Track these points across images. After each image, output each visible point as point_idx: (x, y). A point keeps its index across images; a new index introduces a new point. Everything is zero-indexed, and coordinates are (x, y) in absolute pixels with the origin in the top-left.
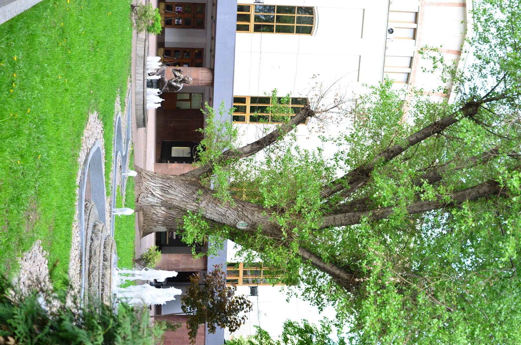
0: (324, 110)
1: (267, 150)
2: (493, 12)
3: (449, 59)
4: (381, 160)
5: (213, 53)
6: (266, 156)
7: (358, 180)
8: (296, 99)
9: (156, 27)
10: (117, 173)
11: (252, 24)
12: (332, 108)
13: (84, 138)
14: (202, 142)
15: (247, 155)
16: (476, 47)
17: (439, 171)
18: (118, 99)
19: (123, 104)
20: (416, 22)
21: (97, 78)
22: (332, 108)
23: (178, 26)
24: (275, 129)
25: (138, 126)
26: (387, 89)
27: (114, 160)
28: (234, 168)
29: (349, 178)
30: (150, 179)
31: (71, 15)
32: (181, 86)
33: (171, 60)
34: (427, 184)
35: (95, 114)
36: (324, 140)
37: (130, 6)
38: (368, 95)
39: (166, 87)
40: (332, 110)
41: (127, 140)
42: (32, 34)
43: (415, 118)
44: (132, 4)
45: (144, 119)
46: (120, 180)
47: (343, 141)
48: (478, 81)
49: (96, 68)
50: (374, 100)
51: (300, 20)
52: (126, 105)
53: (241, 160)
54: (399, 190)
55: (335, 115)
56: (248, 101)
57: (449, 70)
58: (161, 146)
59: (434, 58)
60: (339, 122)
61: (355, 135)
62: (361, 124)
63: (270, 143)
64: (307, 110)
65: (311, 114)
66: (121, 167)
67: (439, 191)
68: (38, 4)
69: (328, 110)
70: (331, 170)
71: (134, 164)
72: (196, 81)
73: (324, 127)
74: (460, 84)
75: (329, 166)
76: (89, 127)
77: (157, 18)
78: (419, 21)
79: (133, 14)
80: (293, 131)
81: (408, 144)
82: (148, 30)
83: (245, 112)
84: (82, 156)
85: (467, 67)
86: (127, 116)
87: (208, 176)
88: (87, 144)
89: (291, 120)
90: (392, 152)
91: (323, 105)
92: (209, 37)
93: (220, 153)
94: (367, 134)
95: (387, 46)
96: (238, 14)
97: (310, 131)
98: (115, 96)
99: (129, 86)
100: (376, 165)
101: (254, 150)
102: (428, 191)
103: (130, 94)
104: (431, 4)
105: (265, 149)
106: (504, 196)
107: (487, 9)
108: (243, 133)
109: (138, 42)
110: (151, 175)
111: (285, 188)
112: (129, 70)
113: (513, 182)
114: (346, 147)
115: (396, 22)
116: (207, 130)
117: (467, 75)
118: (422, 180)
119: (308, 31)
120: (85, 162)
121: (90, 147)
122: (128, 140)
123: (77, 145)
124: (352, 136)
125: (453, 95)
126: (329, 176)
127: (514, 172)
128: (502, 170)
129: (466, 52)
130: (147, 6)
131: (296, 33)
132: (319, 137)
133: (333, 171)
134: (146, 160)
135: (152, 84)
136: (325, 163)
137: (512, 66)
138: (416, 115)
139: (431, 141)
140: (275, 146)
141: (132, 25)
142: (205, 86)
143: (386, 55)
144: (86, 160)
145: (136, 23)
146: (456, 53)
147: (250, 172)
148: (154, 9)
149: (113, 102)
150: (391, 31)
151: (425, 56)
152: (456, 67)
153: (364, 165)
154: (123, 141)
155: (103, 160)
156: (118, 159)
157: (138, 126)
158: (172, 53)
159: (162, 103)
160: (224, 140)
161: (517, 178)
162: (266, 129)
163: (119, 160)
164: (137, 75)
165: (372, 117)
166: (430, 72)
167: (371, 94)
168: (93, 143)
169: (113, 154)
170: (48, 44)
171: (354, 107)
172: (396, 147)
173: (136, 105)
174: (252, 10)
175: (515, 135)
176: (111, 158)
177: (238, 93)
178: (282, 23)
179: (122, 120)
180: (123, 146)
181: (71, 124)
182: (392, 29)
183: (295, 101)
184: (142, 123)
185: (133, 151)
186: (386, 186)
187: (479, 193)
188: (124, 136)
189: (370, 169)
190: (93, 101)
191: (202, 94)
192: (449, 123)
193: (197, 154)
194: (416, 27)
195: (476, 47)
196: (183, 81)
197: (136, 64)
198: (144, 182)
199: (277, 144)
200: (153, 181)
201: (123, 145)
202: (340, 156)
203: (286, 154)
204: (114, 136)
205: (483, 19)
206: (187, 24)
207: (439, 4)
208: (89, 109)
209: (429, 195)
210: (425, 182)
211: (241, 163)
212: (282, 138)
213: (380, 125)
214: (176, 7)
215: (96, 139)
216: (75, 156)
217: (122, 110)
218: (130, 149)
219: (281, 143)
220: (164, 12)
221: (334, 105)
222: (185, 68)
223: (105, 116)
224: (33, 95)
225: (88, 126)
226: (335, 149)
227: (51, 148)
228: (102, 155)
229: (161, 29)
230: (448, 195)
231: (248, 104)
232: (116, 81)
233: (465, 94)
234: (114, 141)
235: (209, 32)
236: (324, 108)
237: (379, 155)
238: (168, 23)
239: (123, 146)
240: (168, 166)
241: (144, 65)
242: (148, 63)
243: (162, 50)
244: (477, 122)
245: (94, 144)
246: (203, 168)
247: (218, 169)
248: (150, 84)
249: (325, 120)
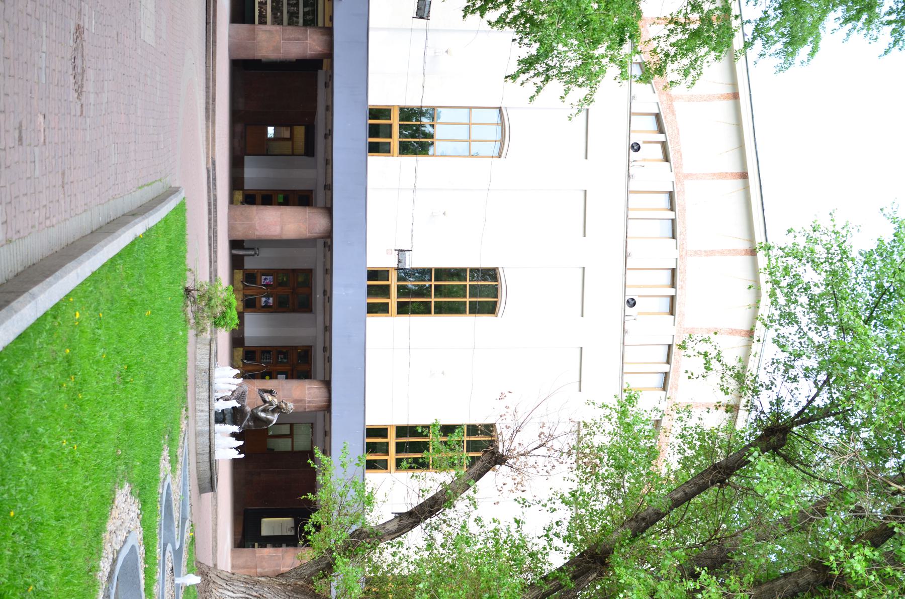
0: (523, 452)
1: (427, 527)
2: (800, 270)
3: (732, 355)
4: (626, 535)
5: (327, 354)
6: (426, 536)
7: (588, 571)
8: (474, 426)
9: (228, 318)
10: (166, 583)
11: (393, 301)
12: (535, 449)
13: (107, 534)
14: (313, 516)
15: (393, 536)
16: (776, 330)
17: (727, 545)
18: (165, 453)
19: (174, 460)
20: (673, 285)
21: (128, 427)
22: (535, 449)
23: (267, 309)
24: (440, 489)
25: (202, 490)
26: (630, 409)
27: (159, 561)
28: (370, 560)
29: (572, 569)
30: (224, 585)
31: (82, 331)
32: (274, 418)
33: (257, 368)
34: (707, 576)
35: (127, 487)
36: (524, 503)
37: (182, 292)
38: (598, 421)
39: (248, 421)
40: (536, 452)
41: (182, 519)
42: (16, 382)
43: (680, 456)
44: (187, 286)
45: (211, 478)
46: (171, 592)
47: (558, 504)
48: (783, 389)
49: (125, 411)
50: (608, 427)
51: (475, 292)
52: (180, 459)
53: (382, 545)
54: (659, 587)
55: (541, 461)
56: (392, 434)
57: (732, 373)
58: (242, 517)
59: (706, 355)
60: (549, 471)
61: (579, 493)
62: (587, 471)
63: (431, 514)
64: (493, 453)
65: (500, 460)
66: (172, 570)
67: (728, 586)
68: (27, 329)
69: (529, 452)
70: (539, 556)
71: (196, 559)
72: (300, 404)
73: (524, 483)
74: (753, 396)
75: (535, 549)
76: (115, 513)
77: (230, 303)
78: (679, 283)
79: (189, 302)
80: (470, 492)
81: (671, 504)
82: (216, 324)
83: (387, 452)
84: (105, 566)
85: (763, 365)
86: (182, 479)
87: (325, 576)
88: (113, 544)
89: (467, 473)
90: (644, 519)
91: (520, 444)
92: (320, 327)
93: (345, 535)
94: (599, 487)
95: (626, 328)
96: (369, 286)
97: (500, 491)
98: (160, 450)
99: (183, 426)
100: (617, 544)
101: (404, 528)
102: (710, 588)
103: (186, 441)
104: (697, 253)
105: (424, 525)
106: (842, 589)
107: (790, 266)
108: (384, 499)
109: (199, 346)
110: (226, 578)
111: (461, 593)
112: (183, 398)
113: (855, 565)
114: (565, 514)
115: (639, 287)
116: (322, 495)
117: (764, 378)
118: (698, 569)
119: (491, 309)
120: (110, 577)
121: (118, 548)
122: (184, 519)
123: (94, 550)
124: (573, 495)
125: (742, 414)
126: (536, 567)
127: (855, 546)
128: (833, 544)
129: (759, 341)
130: (213, 289)
131: (470, 313)
132: (516, 500)
133: (543, 559)
134: (216, 546)
135: (224, 416)
136: (529, 545)
137: (838, 364)
138: (681, 451)
139: (710, 495)
140: (441, 519)
141: (187, 321)
142: (316, 411)
143: (625, 344)
144: (111, 572)
145: (195, 319)
146: (745, 334)
147: (399, 564)
148: (224, 288)
149: (157, 461)
150: (632, 303)
151: (690, 352)
152: (744, 368)
153: (596, 545)
154: (176, 523)
155: (141, 565)
156: (166, 557)
157: (202, 490)
158: (258, 355)
159: (240, 449)
160: (351, 512)
161: (860, 557)
162: (423, 491)
163: (170, 559)
164: (197, 402)
165: (606, 458)
166: (701, 377)
167: (603, 419)
168: (123, 539)
169: (158, 551)
170: (43, 391)
171: (574, 443)
172: (650, 511)
173: (197, 454)
174: (393, 276)
175: (852, 483)
176: (155, 558)
177: (374, 420)
178: (445, 297)
179: (173, 488)
180: (176, 533)
181: (84, 518)
182: (633, 299)
183: (473, 429)
184: (208, 485)
185: (193, 539)
186: (636, 582)
187: (798, 585)
188: (176, 515)
189: (608, 552)
190: (123, 467)
191: (312, 424)
192: (739, 465)
193: (304, 537)
194: (674, 294)
195: (776, 330)
196: (278, 409)
197: (196, 383)
198: (213, 590)
199: (444, 515)
200: (229, 588)
201: (176, 531)
202: (553, 531)
203: (459, 532)
204: (160, 519)
205: (784, 283)
206: (283, 306)
207: (711, 253)
208: (115, 483)
209: (711, 595)
210: (703, 572)
211: (383, 549)
212: (451, 506)
213: (621, 468)
214: (263, 277)
215: (129, 532)
216: (92, 570)
217: (173, 471)
218: (187, 535)
219: (450, 513)
220: (242, 286)
221: (539, 443)
222: (280, 381)
223: (143, 488)
224: (20, 486)
225: (113, 512)
226: (547, 519)
227: (50, 569)
228: (139, 556)
229: (237, 321)
230: (744, 591)
231: (392, 440)
232: (161, 425)
233: (762, 412)
234: (161, 528)
235: (320, 318)
236: (521, 450)
237: (622, 526)
238: (249, 304)
239: (176, 533)
240: (255, 553)
241: (210, 384)
242: (216, 381)
243: (240, 352)
244: (789, 460)
245: (125, 542)
246: (317, 563)
247: (343, 565)
248: (221, 418)
249: (525, 469)
